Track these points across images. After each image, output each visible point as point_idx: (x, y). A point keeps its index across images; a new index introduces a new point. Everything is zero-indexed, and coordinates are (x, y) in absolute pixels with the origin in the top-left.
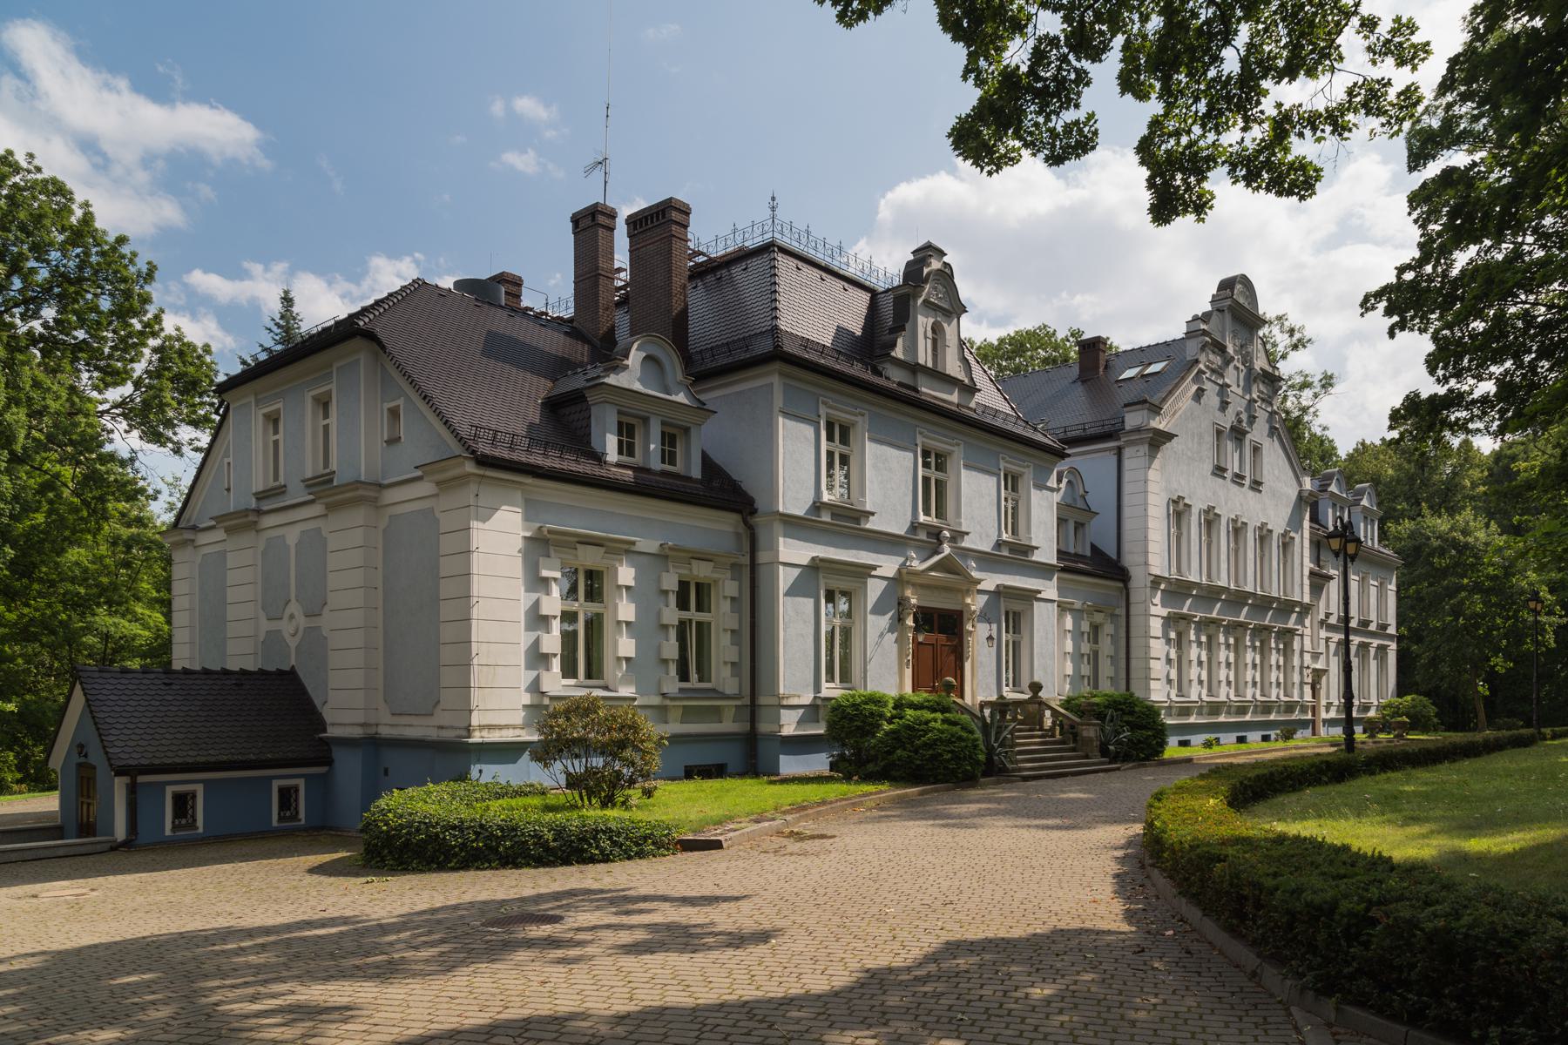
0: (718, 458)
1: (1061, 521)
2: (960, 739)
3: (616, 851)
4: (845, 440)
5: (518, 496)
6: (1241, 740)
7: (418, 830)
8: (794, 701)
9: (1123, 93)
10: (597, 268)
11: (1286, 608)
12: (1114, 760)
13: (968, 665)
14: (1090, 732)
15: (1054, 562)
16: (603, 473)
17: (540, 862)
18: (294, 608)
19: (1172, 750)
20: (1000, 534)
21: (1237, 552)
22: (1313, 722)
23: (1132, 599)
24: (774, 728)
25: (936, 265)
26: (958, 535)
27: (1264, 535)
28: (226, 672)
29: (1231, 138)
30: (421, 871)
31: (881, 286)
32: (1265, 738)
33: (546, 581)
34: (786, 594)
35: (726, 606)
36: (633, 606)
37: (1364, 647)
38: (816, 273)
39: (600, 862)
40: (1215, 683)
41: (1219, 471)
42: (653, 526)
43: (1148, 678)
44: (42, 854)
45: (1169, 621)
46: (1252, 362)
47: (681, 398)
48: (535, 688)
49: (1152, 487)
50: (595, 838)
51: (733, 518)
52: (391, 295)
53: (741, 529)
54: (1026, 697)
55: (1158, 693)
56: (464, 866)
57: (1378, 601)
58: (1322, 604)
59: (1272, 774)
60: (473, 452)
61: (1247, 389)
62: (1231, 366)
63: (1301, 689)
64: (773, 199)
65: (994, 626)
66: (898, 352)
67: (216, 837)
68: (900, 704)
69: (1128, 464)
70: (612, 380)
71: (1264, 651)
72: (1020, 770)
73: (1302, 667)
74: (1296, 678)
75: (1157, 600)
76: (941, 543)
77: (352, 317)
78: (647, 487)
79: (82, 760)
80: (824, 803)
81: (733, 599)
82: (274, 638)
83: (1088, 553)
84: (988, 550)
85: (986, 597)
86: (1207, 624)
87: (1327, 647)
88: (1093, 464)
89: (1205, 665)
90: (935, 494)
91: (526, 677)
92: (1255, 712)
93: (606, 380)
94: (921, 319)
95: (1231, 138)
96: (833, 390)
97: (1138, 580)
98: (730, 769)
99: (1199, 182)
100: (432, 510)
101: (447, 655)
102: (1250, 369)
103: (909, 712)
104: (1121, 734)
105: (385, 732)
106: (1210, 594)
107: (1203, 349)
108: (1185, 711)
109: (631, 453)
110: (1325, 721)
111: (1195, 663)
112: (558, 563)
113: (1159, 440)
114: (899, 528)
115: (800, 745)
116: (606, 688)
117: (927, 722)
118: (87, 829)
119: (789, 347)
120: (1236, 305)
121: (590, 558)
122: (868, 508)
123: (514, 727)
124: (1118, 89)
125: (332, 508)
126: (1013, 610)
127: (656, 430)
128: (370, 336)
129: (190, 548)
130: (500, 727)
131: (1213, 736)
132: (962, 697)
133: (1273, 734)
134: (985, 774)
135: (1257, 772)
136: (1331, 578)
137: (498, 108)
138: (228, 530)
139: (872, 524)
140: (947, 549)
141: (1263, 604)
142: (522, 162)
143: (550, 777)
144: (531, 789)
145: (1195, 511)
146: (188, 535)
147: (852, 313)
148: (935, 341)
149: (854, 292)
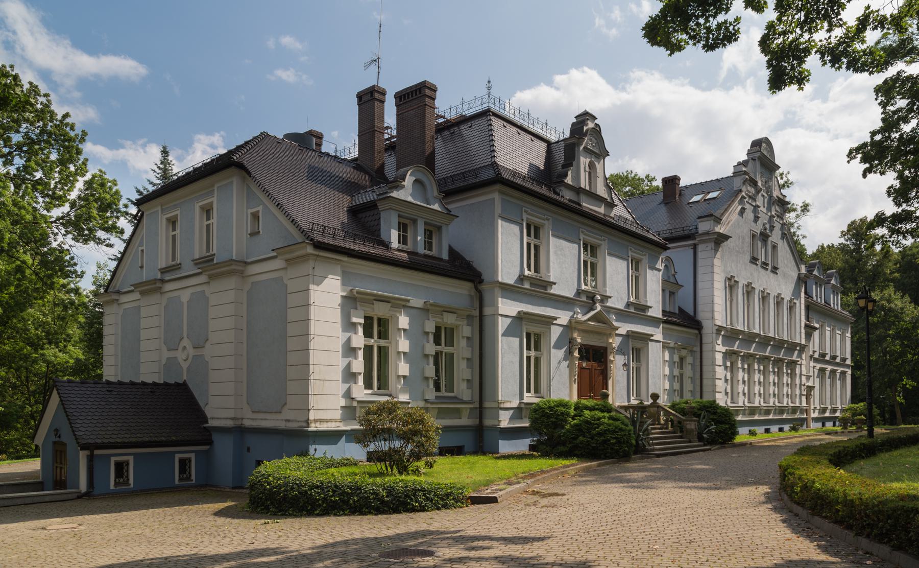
0: (457, 248)
2: (621, 429)
3: (429, 504)
4: (537, 236)
5: (339, 269)
7: (292, 488)
8: (508, 405)
9: (746, 8)
10: (374, 126)
11: (792, 347)
13: (610, 382)
14: (691, 425)
15: (660, 316)
16: (389, 254)
17: (378, 511)
18: (186, 342)
19: (743, 435)
20: (629, 298)
23: (704, 341)
24: (495, 423)
25: (591, 125)
26: (605, 298)
27: (779, 301)
28: (144, 384)
29: (820, 36)
30: (296, 516)
31: (553, 138)
33: (354, 324)
34: (503, 335)
35: (464, 343)
36: (408, 342)
37: (833, 372)
38: (515, 130)
39: (418, 511)
40: (752, 395)
41: (754, 260)
42: (419, 290)
44: (36, 500)
45: (727, 355)
46: (771, 192)
47: (436, 207)
48: (348, 395)
49: (716, 270)
52: (254, 138)
53: (473, 292)
55: (722, 400)
56: (325, 513)
57: (839, 342)
60: (312, 240)
61: (769, 209)
63: (800, 398)
64: (489, 82)
66: (569, 180)
67: (142, 491)
69: (700, 255)
70: (395, 194)
71: (779, 374)
73: (801, 385)
74: (798, 392)
75: (720, 342)
76: (595, 303)
77: (230, 153)
78: (417, 264)
79: (57, 439)
80: (543, 472)
81: (468, 338)
82: (171, 361)
83: (677, 312)
88: (680, 254)
89: (729, 382)
91: (343, 388)
92: (775, 414)
93: (391, 195)
94: (582, 159)
95: (820, 36)
97: (708, 328)
98: (466, 450)
99: (799, 65)
100: (203, 292)
101: (291, 373)
102: (771, 197)
103: (586, 412)
105: (248, 423)
106: (750, 338)
110: (813, 419)
111: (741, 382)
112: (362, 314)
113: (721, 239)
114: (570, 293)
115: (512, 433)
116: (390, 395)
117: (599, 419)
118: (60, 484)
119: (505, 175)
120: (762, 156)
121: (380, 310)
122: (551, 280)
123: (336, 421)
124: (743, 5)
125: (212, 277)
126: (636, 346)
127: (421, 227)
128: (240, 166)
129: (115, 305)
130: (327, 421)
134: (636, 453)
136: (816, 329)
137: (271, 43)
138: (142, 293)
139: (554, 290)
140: (599, 307)
141: (779, 344)
142: (287, 75)
143: (356, 452)
144: (349, 461)
145: (740, 285)
146: (114, 297)
147: (537, 156)
148: (590, 173)
149: (538, 143)
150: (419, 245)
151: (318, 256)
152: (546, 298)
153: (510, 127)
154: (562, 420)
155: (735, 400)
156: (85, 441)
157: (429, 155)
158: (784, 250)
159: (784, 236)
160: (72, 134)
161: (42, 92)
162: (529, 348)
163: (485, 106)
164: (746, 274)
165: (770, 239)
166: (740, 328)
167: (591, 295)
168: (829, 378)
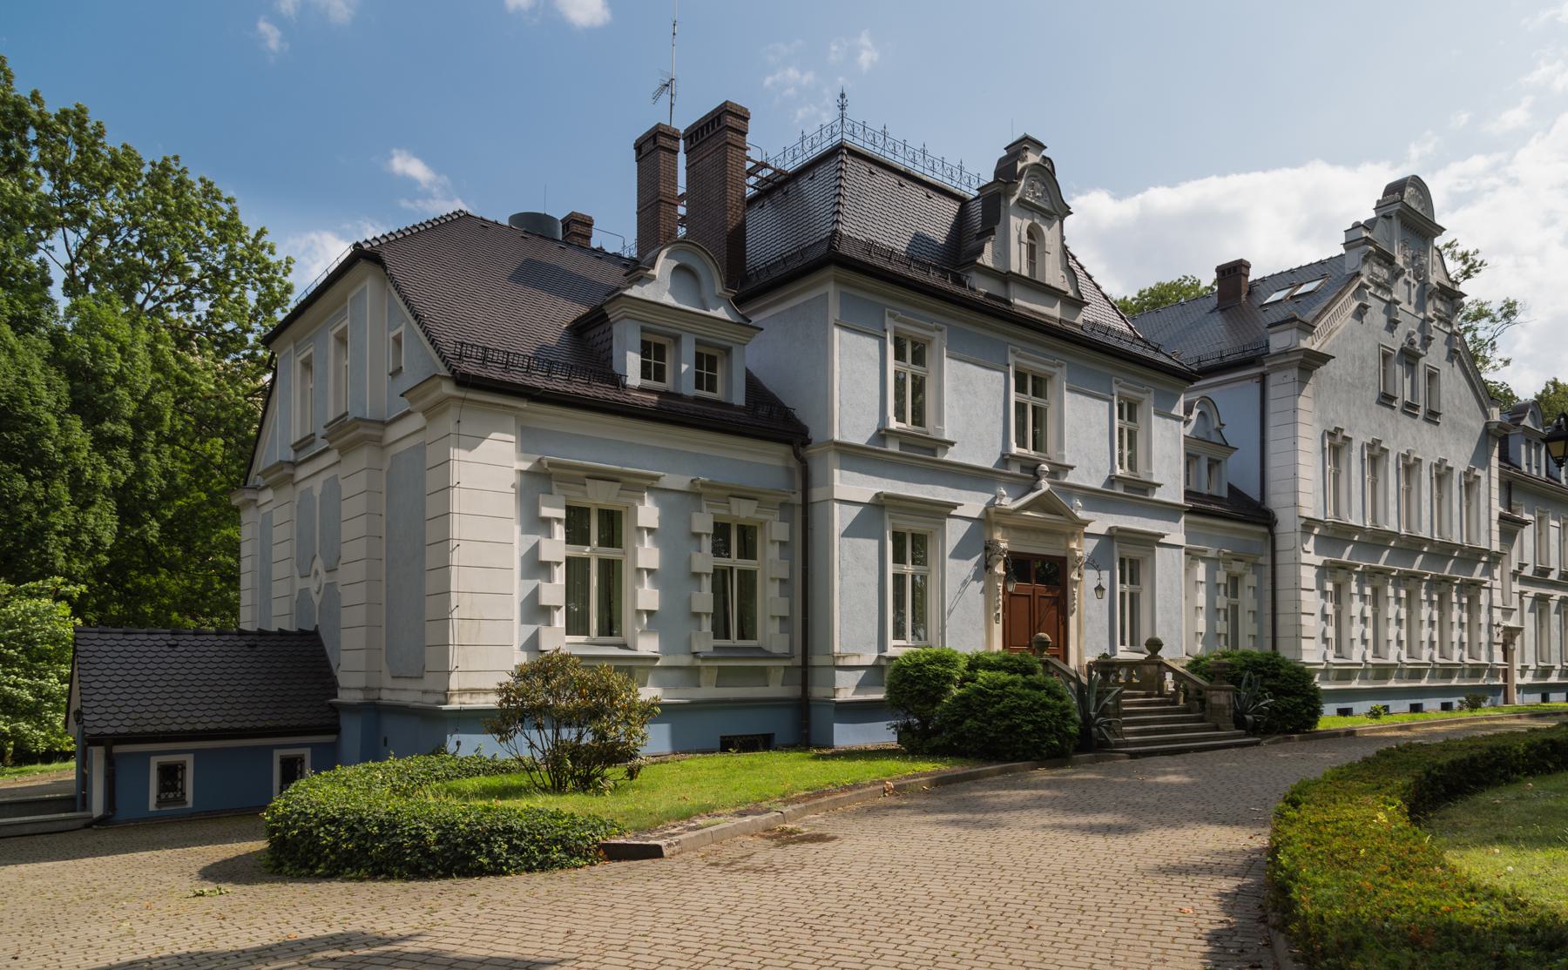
0: (770, 383)
1: (1191, 458)
2: (1044, 706)
4: (919, 358)
6: (1416, 708)
11: (1471, 556)
12: (1254, 730)
13: (1073, 620)
14: (1221, 699)
15: (1181, 501)
16: (620, 397)
19: (1329, 719)
21: (1408, 493)
22: (1505, 687)
23: (1279, 546)
24: (829, 692)
25: (1032, 158)
27: (1442, 474)
32: (1446, 707)
33: (547, 522)
35: (773, 552)
41: (1386, 399)
42: (681, 459)
43: (1298, 637)
45: (1324, 571)
46: (1426, 276)
47: (721, 313)
48: (532, 644)
50: (487, 841)
51: (782, 450)
53: (793, 463)
54: (1142, 657)
55: (1312, 653)
56: (332, 874)
58: (1515, 552)
59: (1473, 759)
61: (1421, 306)
62: (1401, 280)
64: (843, 96)
65: (1106, 574)
66: (987, 259)
68: (975, 664)
69: (1272, 392)
70: (635, 291)
71: (1443, 605)
72: (1128, 744)
73: (1490, 625)
74: (1484, 638)
76: (1038, 478)
78: (671, 413)
81: (782, 543)
83: (1225, 494)
84: (1099, 487)
85: (1096, 541)
86: (1373, 576)
87: (1521, 602)
88: (1233, 399)
89: (1370, 622)
90: (1033, 422)
92: (1432, 677)
96: (903, 301)
97: (1287, 524)
98: (777, 741)
102: (1424, 284)
103: (982, 674)
104: (1262, 698)
105: (387, 697)
106: (1376, 540)
107: (1365, 260)
108: (1346, 675)
109: (660, 377)
110: (1519, 687)
111: (1357, 619)
113: (1311, 362)
114: (988, 461)
116: (624, 646)
117: (1003, 686)
119: (845, 250)
121: (598, 496)
122: (946, 437)
126: (1130, 558)
127: (688, 349)
131: (1381, 703)
132: (1066, 661)
133: (1455, 702)
134: (1079, 750)
135: (1451, 756)
136: (1526, 523)
140: (1045, 485)
141: (1442, 551)
145: (1356, 445)
147: (938, 221)
149: (938, 200)
150: (684, 380)
151: (464, 399)
152: (935, 470)
153: (883, 177)
154: (935, 688)
155: (1382, 653)
156: (96, 731)
157: (733, 231)
158: (1452, 382)
159: (1452, 355)
160: (272, 259)
161: (225, 196)
162: (1122, 581)
163: (836, 139)
164: (1364, 425)
165: (1422, 361)
166: (1355, 521)
167: (1032, 464)
168: (1558, 611)
